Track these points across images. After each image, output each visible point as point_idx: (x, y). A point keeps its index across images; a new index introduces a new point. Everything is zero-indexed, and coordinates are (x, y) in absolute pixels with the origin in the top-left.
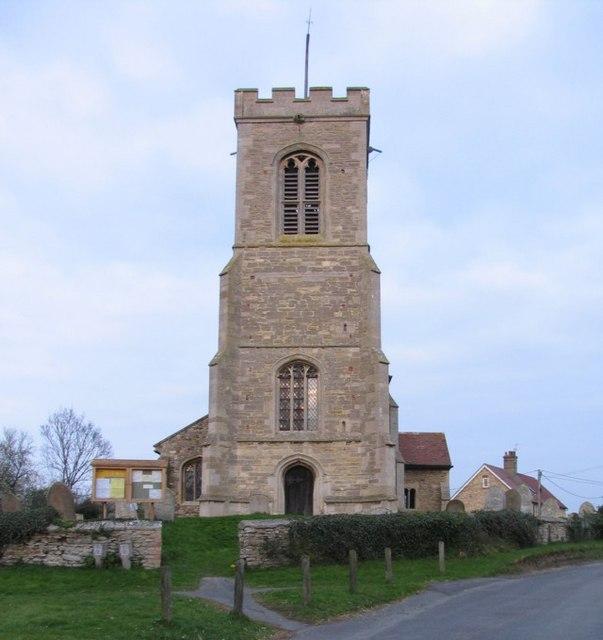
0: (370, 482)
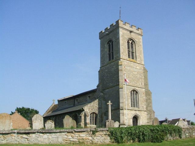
0: (150, 121)
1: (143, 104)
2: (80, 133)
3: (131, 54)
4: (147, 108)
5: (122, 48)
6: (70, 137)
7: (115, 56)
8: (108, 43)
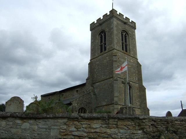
1: (137, 100)
2: (90, 121)
3: (124, 47)
4: (140, 105)
5: (116, 38)
6: (73, 129)
7: (107, 47)
8: (99, 34)
